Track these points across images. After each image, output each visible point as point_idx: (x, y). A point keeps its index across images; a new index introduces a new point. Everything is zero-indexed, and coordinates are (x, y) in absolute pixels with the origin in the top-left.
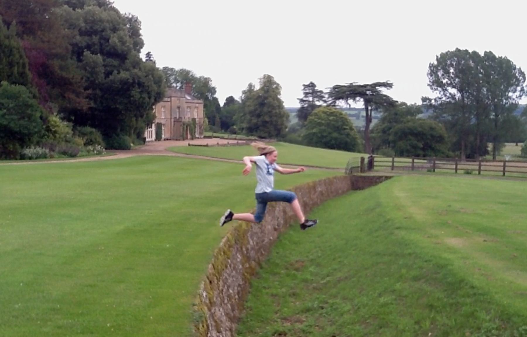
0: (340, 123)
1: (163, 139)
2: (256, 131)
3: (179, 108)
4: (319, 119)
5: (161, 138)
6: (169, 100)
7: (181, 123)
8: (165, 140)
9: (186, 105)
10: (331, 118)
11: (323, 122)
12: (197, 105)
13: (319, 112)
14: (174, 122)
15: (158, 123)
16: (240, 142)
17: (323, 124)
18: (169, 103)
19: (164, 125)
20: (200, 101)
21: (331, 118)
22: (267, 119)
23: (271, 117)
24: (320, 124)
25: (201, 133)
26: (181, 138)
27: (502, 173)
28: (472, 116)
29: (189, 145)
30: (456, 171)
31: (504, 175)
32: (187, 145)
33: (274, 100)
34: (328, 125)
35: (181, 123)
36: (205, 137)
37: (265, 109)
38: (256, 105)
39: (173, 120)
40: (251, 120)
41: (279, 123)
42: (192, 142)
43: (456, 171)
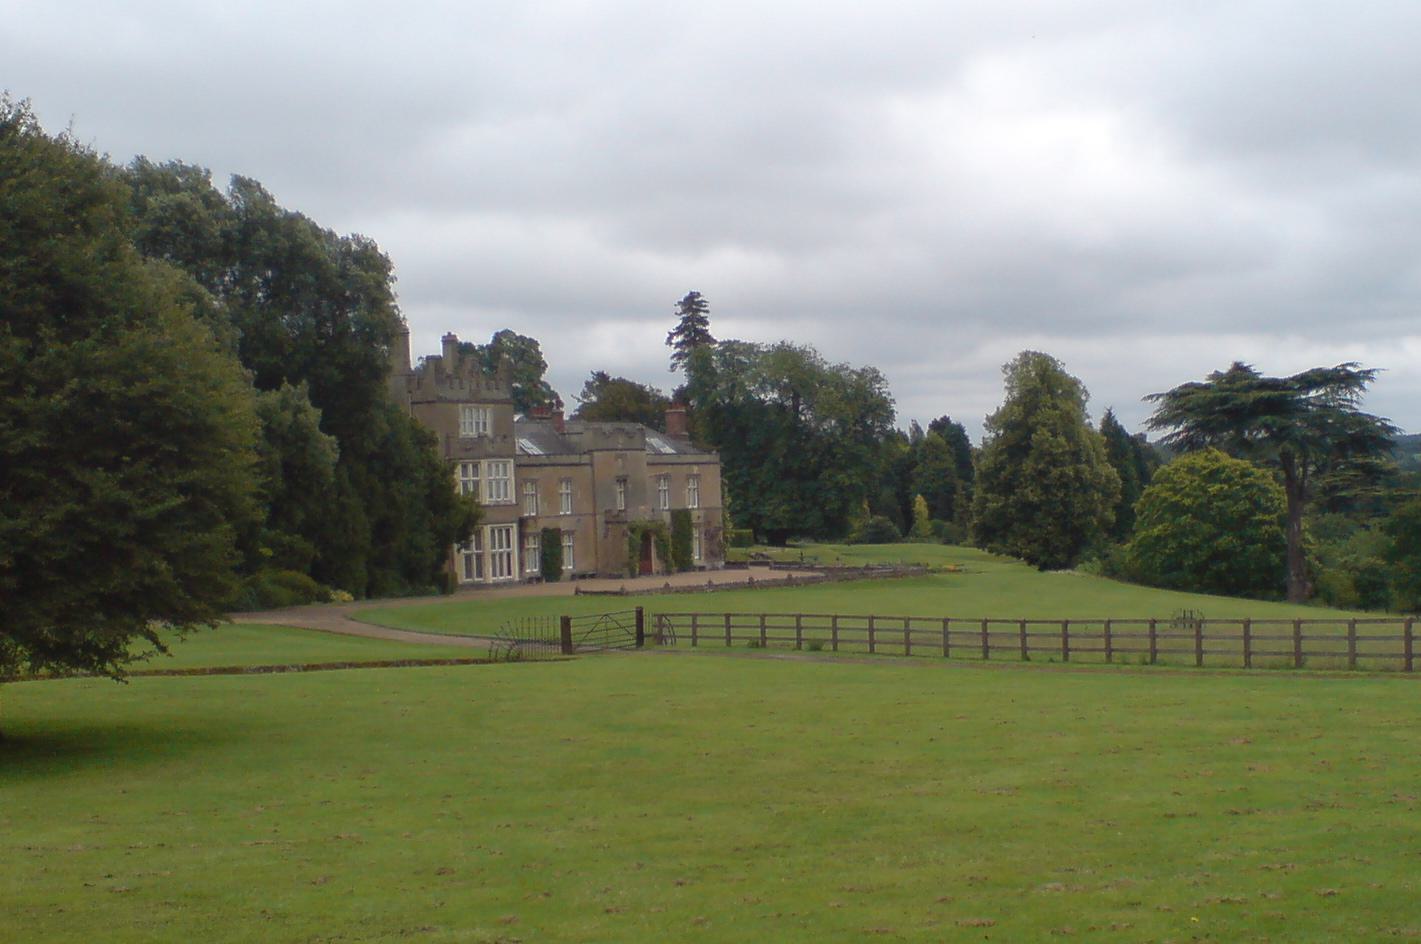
0: (1244, 505)
1: (566, 575)
2: (1004, 538)
3: (622, 480)
4: (1176, 491)
5: (560, 572)
6: (585, 459)
7: (625, 527)
8: (574, 577)
9: (648, 473)
10: (1214, 488)
11: (1187, 502)
12: (696, 469)
13: (1177, 470)
14: (607, 522)
15: (545, 531)
16: (795, 574)
17: (1185, 510)
18: (588, 469)
19: (570, 533)
20: (706, 458)
21: (1214, 488)
22: (1032, 495)
23: (1046, 489)
24: (1177, 509)
25: (711, 554)
26: (626, 570)
27: (867, 648)
28: (1273, 504)
29: (577, 592)
30: (729, 643)
31: (872, 650)
32: (573, 592)
33: (1055, 435)
34: (1201, 513)
35: (625, 527)
36: (730, 565)
37: (1028, 466)
38: (1001, 453)
39: (600, 519)
40: (987, 500)
41: (1078, 508)
42: (679, 580)
43: (729, 643)
